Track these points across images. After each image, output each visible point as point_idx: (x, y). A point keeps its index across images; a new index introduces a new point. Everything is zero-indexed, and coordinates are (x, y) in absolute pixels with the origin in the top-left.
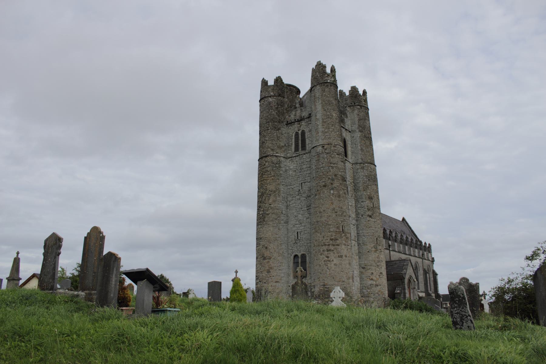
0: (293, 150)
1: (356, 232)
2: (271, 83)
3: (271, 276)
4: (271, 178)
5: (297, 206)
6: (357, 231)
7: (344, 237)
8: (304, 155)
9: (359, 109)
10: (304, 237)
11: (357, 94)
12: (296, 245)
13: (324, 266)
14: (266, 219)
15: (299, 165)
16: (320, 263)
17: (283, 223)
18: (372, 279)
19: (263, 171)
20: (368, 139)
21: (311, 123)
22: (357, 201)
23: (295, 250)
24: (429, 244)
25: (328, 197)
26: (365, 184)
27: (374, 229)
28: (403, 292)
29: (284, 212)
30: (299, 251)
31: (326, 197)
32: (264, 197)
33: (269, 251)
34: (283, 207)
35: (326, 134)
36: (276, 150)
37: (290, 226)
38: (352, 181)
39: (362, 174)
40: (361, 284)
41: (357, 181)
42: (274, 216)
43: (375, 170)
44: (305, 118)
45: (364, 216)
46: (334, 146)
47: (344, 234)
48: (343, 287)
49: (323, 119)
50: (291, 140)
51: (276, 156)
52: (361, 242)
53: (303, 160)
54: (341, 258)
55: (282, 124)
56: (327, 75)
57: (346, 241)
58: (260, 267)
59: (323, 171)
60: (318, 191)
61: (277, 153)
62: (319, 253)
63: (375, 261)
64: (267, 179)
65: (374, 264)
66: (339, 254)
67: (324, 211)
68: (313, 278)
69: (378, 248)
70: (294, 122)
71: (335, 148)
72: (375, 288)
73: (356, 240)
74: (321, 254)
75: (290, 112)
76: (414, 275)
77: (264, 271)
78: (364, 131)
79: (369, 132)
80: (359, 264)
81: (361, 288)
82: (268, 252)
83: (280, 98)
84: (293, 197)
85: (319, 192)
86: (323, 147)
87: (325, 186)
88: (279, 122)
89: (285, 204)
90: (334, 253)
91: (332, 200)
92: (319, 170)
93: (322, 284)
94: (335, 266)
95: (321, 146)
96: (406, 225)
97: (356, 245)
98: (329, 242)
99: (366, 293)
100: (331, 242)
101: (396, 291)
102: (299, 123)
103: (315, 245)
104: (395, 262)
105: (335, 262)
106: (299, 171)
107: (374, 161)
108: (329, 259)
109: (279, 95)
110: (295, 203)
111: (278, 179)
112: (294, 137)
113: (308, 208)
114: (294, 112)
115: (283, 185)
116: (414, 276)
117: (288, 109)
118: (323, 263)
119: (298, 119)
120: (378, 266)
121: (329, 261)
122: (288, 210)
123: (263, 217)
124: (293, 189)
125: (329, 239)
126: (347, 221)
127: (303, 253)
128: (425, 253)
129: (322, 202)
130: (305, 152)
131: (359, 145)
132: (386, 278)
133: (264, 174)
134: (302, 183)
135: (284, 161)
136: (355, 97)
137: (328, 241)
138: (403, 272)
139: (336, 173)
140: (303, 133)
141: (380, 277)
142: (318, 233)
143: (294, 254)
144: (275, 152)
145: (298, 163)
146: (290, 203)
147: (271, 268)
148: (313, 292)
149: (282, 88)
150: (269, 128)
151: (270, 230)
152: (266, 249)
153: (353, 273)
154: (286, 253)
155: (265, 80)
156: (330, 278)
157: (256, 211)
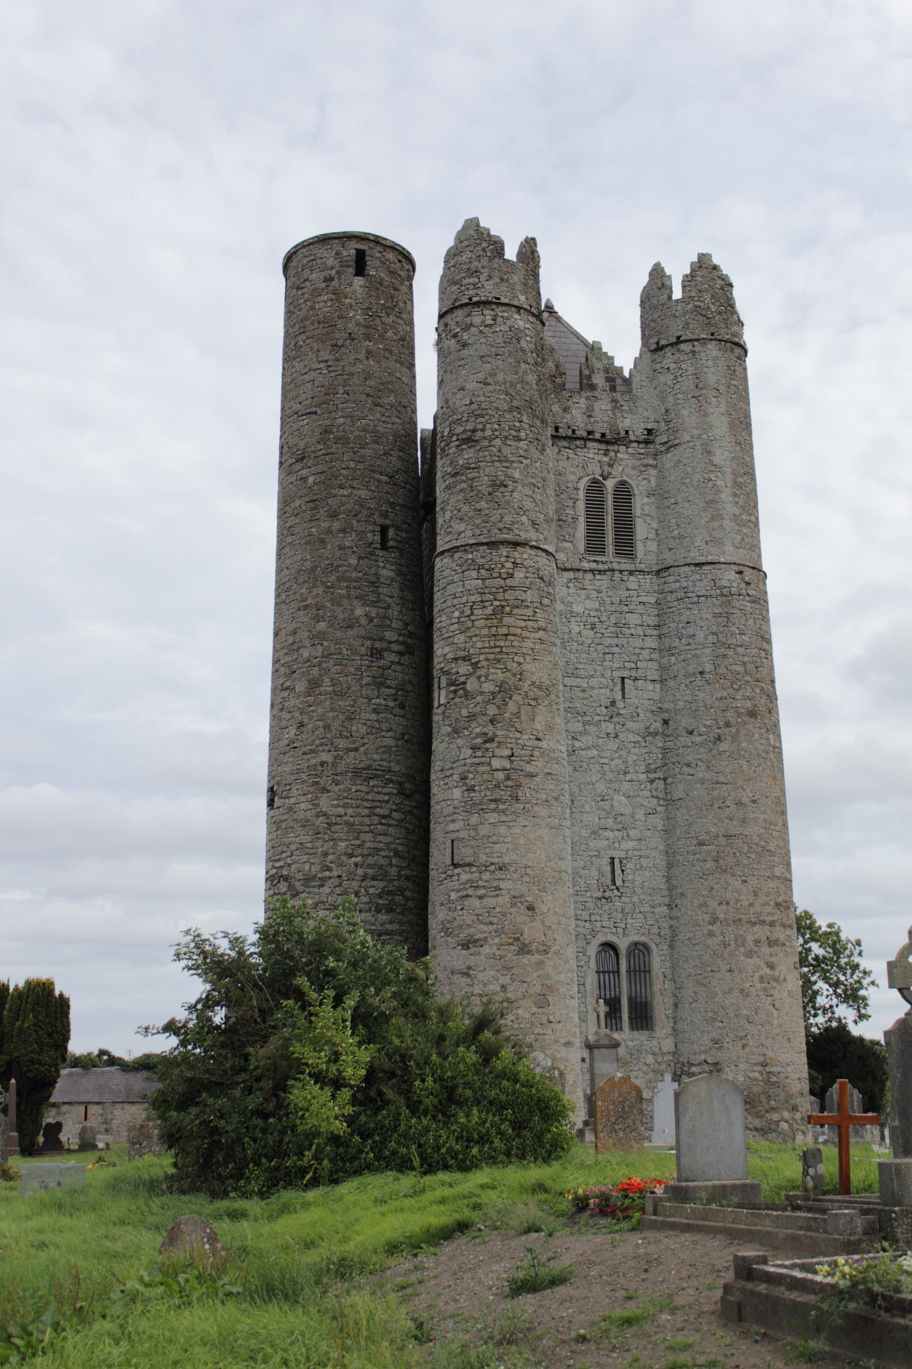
0: (581, 545)
3: (551, 1018)
5: (606, 761)
13: (763, 997)
14: (525, 793)
15: (609, 608)
16: (747, 985)
30: (620, 930)
31: (759, 755)
33: (543, 923)
50: (570, 503)
62: (742, 950)
67: (754, 802)
70: (585, 440)
74: (749, 954)
82: (537, 924)
85: (734, 730)
92: (730, 653)
102: (603, 446)
108: (776, 973)
113: (652, 776)
114: (583, 400)
118: (758, 986)
121: (776, 980)
124: (584, 691)
125: (772, 903)
127: (636, 938)
129: (745, 767)
133: (510, 614)
134: (623, 679)
140: (624, 493)
142: (733, 875)
143: (601, 938)
145: (608, 601)
151: (540, 837)
152: (530, 913)
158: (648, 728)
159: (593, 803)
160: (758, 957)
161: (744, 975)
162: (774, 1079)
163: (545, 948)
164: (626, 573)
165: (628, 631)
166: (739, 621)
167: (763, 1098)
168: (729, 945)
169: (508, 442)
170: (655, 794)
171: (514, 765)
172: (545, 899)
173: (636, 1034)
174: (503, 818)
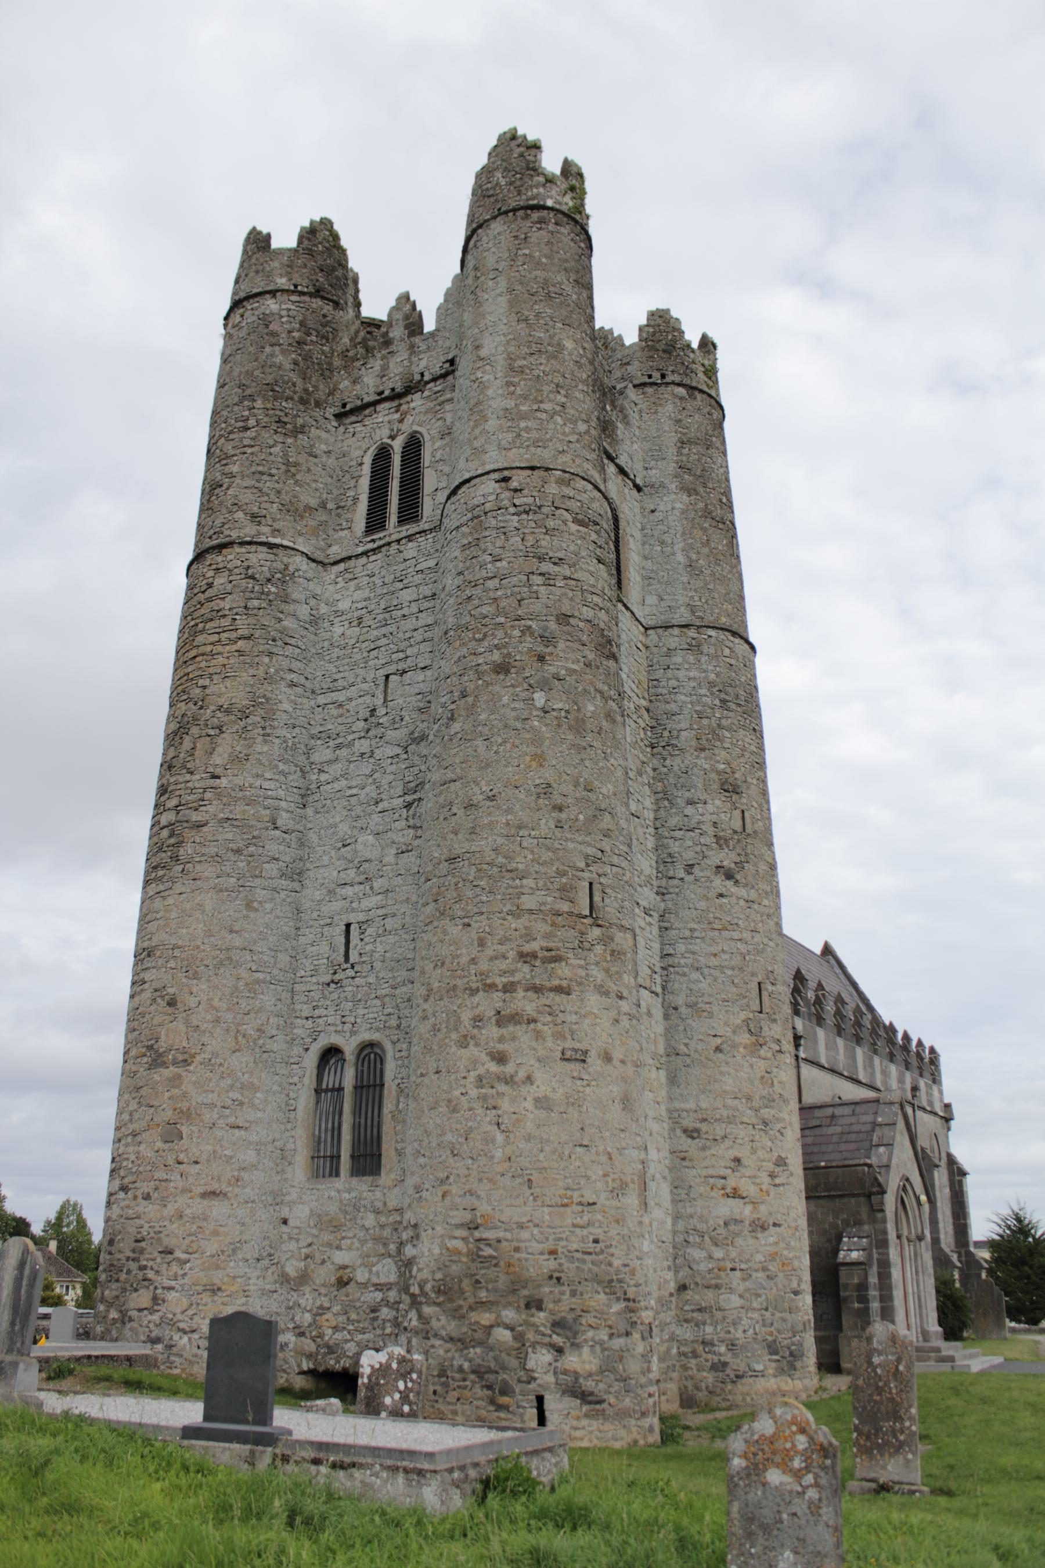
1: (656, 946)
2: (285, 239)
4: (235, 647)
5: (354, 791)
6: (662, 944)
7: (599, 949)
8: (410, 544)
9: (681, 398)
10: (380, 948)
11: (674, 341)
12: (335, 996)
13: (480, 1111)
14: (187, 851)
15: (379, 591)
16: (457, 1093)
17: (275, 873)
18: (735, 1194)
19: (196, 614)
20: (721, 526)
21: (451, 400)
22: (663, 797)
23: (330, 1020)
24: (932, 1050)
25: (519, 725)
26: (705, 722)
27: (746, 935)
28: (875, 1256)
29: (284, 819)
32: (187, 739)
33: (187, 1022)
34: (281, 793)
35: (523, 424)
36: (274, 520)
37: (312, 893)
38: (644, 703)
39: (691, 674)
40: (677, 1217)
41: (669, 707)
42: (228, 833)
43: (749, 666)
44: (427, 378)
45: (696, 870)
46: (561, 482)
47: (596, 932)
48: (583, 1240)
49: (511, 358)
51: (271, 546)
52: (680, 1000)
53: (402, 566)
54: (575, 1068)
55: (317, 413)
56: (541, 179)
57: (607, 971)
58: (133, 1105)
59: (499, 593)
60: (464, 695)
61: (276, 532)
62: (454, 1036)
63: (749, 1098)
64: (212, 654)
65: (749, 1116)
66: (569, 1044)
67: (491, 798)
68: (411, 1181)
69: (766, 1032)
71: (568, 491)
72: (751, 1241)
73: (659, 990)
75: (358, 364)
76: (917, 1173)
77: (148, 1128)
78: (701, 490)
79: (724, 500)
80: (670, 1111)
81: (680, 1238)
83: (316, 303)
84: (339, 747)
85: (470, 699)
86: (506, 480)
87: (502, 668)
88: (303, 401)
89: (295, 779)
90: (538, 1035)
91: (537, 740)
92: (478, 591)
93: (461, 1216)
94: (543, 1114)
95: (496, 476)
96: (838, 971)
97: (658, 1013)
98: (512, 972)
99: (703, 1267)
100: (526, 968)
101: (842, 1254)
102: (396, 403)
103: (430, 990)
104: (829, 1111)
105: (542, 1086)
106: (380, 617)
107: (744, 624)
108: (509, 1069)
109: (317, 293)
110: (345, 775)
111: (270, 654)
112: (367, 469)
113: (409, 798)
115: (292, 685)
116: (919, 1178)
117: (351, 354)
118: (474, 1092)
119: (393, 389)
120: (766, 1123)
121: (509, 1080)
122: (309, 811)
123: (172, 841)
124: (341, 706)
125: (512, 954)
126: (615, 860)
127: (366, 1036)
128: (922, 1084)
129: (482, 749)
130: (417, 529)
131: (681, 545)
132: (802, 1186)
134: (387, 677)
135: (309, 575)
136: (664, 351)
137: (503, 965)
138: (873, 1160)
139: (566, 608)
140: (414, 447)
141: (777, 1181)
143: (323, 1042)
144: (266, 530)
145: (379, 582)
146: (324, 777)
147: (187, 1115)
148: (409, 1263)
149: (334, 269)
150: (252, 422)
151: (200, 906)
152: (170, 1010)
153: (643, 1156)
154: (280, 1037)
155: (260, 233)
156: (506, 1181)
157: (150, 812)
158: (412, 733)
159: (333, 852)
160: (477, 1045)
161: (453, 1077)
162: (488, 1251)
163: (186, 1056)
164: (404, 541)
165: (399, 613)
166: (493, 544)
167: (466, 1284)
168: (439, 1030)
169: (232, 436)
170: (411, 822)
171: (180, 817)
172: (194, 990)
173: (355, 1180)
174: (161, 887)
